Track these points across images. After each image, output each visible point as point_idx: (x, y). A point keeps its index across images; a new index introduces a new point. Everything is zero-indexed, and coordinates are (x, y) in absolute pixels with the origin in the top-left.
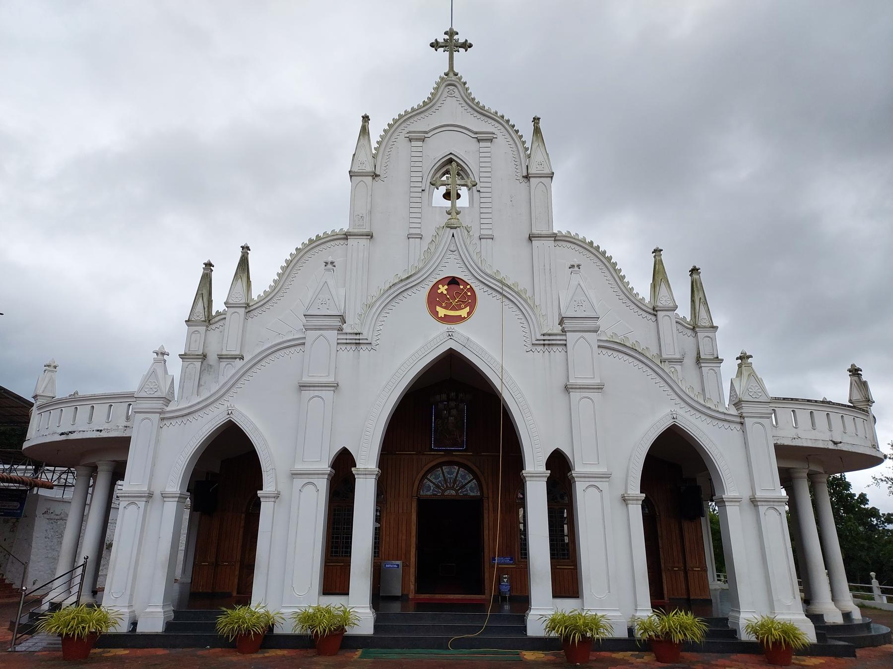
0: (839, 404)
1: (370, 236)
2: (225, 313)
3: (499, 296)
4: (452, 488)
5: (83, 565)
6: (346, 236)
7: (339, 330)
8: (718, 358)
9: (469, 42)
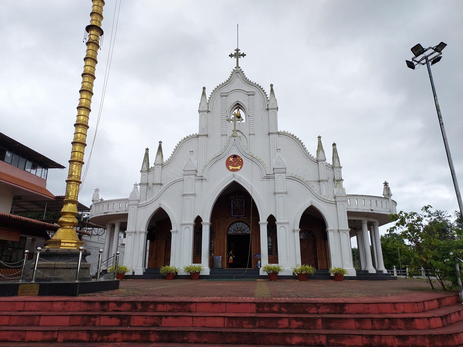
0: (375, 196)
1: (207, 136)
2: (154, 167)
5: (113, 257)
6: (198, 136)
7: (195, 175)
8: (342, 179)
9: (244, 53)
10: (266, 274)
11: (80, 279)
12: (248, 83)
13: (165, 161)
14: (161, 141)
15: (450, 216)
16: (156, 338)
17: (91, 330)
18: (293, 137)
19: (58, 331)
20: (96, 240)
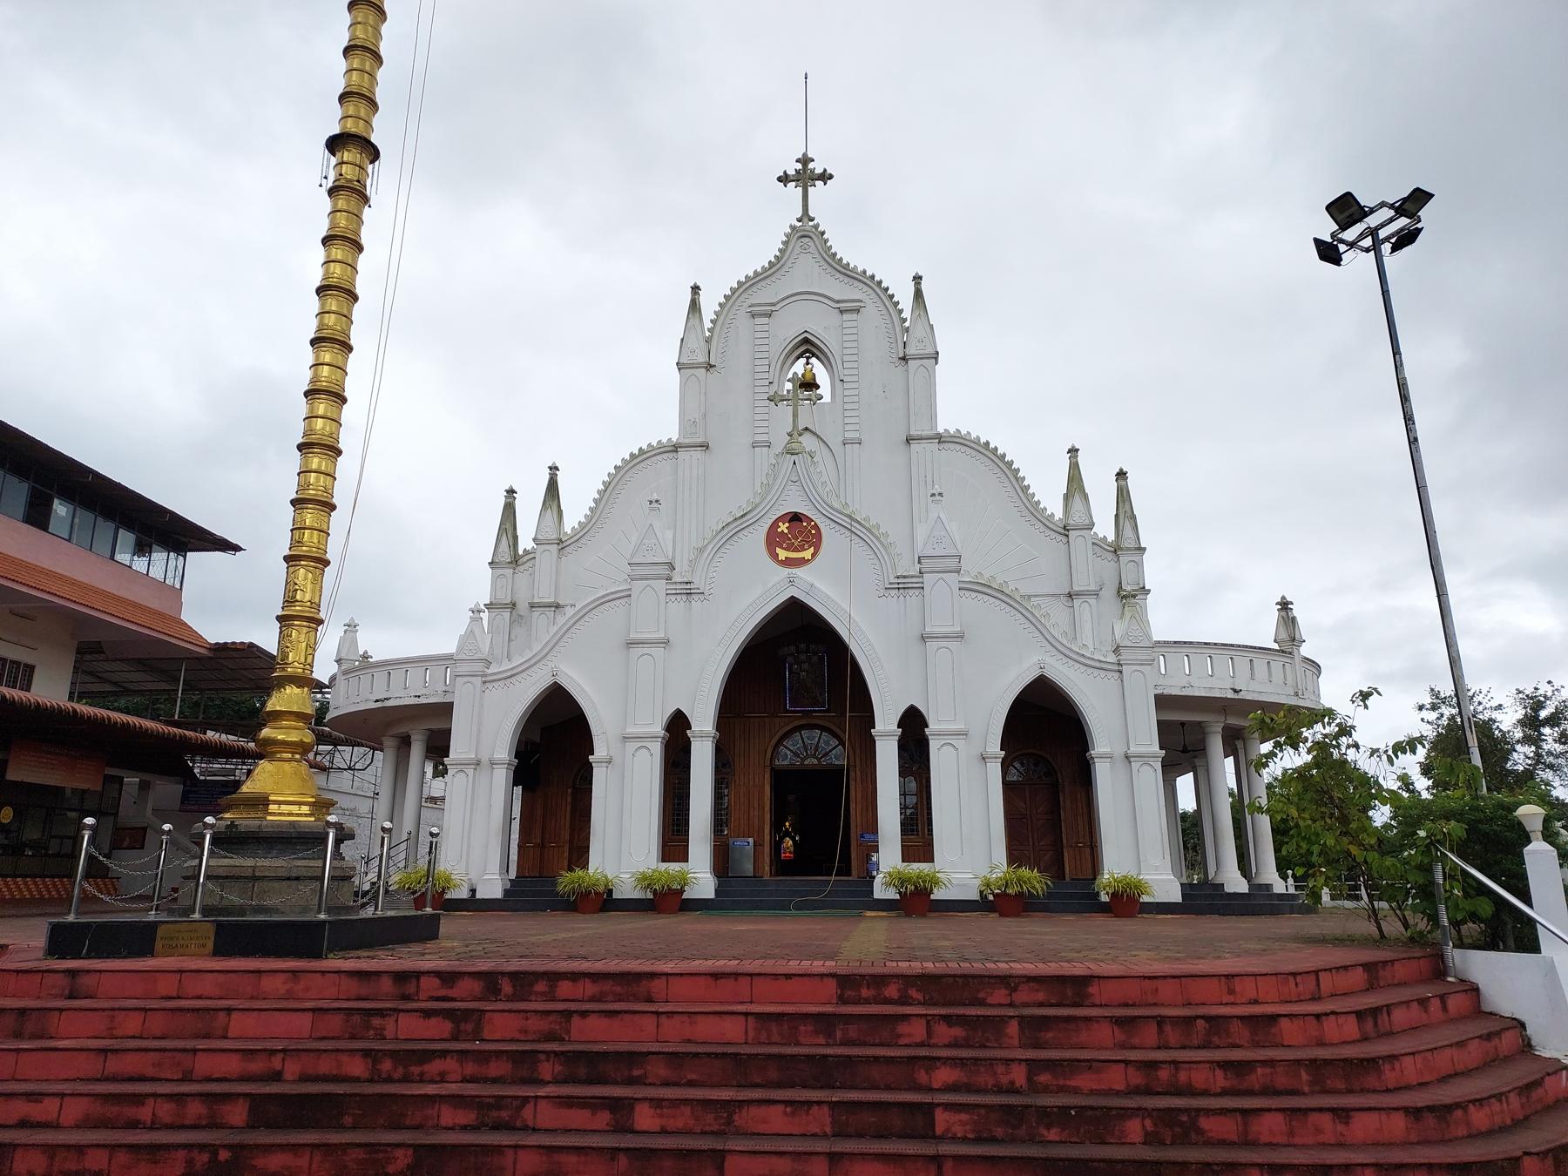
2: (533, 551)
3: (849, 533)
4: (814, 756)
6: (675, 448)
7: (667, 579)
8: (1144, 588)
9: (828, 172)
10: (892, 894)
11: (329, 911)
12: (839, 272)
13: (568, 528)
14: (557, 465)
15: (1501, 705)
16: (556, 1071)
17: (374, 1050)
18: (986, 450)
19: (284, 1051)
20: (346, 786)
